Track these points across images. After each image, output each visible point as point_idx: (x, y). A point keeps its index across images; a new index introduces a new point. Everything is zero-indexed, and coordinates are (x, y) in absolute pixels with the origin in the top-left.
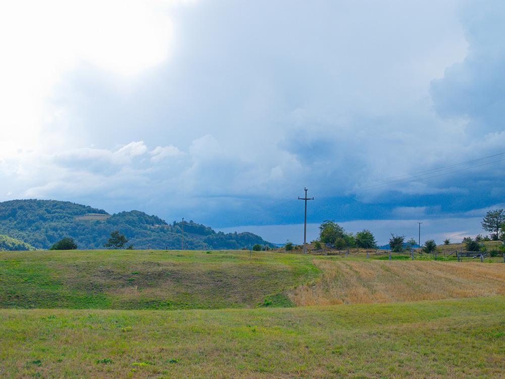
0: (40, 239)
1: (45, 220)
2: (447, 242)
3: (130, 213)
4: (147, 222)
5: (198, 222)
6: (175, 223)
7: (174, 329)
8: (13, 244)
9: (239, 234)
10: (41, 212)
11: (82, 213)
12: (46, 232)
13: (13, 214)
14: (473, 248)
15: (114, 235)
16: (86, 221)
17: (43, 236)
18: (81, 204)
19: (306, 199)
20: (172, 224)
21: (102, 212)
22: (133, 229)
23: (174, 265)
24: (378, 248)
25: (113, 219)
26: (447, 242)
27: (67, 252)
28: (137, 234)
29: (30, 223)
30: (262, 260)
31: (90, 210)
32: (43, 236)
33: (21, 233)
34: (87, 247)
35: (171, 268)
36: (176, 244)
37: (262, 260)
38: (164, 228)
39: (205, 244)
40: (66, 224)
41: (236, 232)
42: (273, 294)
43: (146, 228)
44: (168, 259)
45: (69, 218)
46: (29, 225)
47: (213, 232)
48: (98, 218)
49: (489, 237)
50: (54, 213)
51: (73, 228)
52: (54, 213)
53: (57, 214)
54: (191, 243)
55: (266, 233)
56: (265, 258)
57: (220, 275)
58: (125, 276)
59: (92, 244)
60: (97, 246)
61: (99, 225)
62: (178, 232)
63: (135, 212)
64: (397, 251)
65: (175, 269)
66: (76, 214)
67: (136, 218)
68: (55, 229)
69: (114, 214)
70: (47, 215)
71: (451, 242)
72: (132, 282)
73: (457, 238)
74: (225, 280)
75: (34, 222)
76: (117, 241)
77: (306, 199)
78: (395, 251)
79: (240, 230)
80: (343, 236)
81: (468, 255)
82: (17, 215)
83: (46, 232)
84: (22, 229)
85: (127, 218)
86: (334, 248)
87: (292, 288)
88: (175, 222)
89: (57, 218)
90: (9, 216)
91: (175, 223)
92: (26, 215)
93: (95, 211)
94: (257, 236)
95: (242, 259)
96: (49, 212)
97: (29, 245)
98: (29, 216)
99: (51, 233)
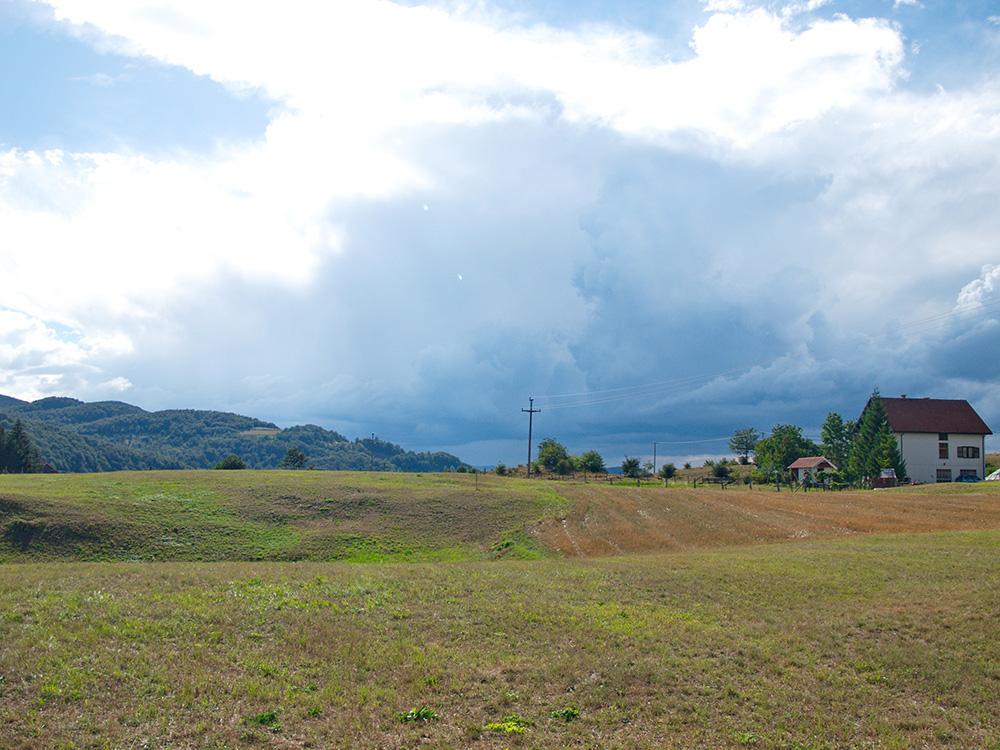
0: (197, 456)
1: (203, 434)
2: (688, 466)
3: (304, 428)
4: (325, 439)
5: (384, 439)
6: (357, 441)
7: (491, 615)
8: (166, 462)
9: (826, 440)
10: (199, 425)
11: (249, 428)
12: (205, 448)
13: (167, 425)
14: (721, 474)
15: (291, 453)
16: (252, 436)
17: (201, 453)
18: (246, 415)
19: (531, 412)
20: (354, 441)
21: (271, 426)
22: (307, 445)
23: (379, 491)
24: (605, 471)
25: (284, 434)
26: (688, 466)
27: (846, 500)
28: (313, 452)
29: (186, 437)
30: (489, 486)
31: (257, 424)
32: (201, 453)
33: (175, 449)
34: (253, 467)
35: (374, 495)
36: (357, 465)
37: (489, 486)
38: (344, 445)
39: (393, 465)
40: (228, 440)
41: (429, 453)
42: (512, 531)
43: (323, 446)
44: (366, 481)
45: (232, 432)
46: (185, 440)
47: (402, 451)
48: (266, 433)
49: (737, 460)
50: (214, 426)
51: (236, 445)
52: (214, 426)
53: (218, 427)
54: (377, 464)
55: (467, 454)
56: (493, 484)
57: (439, 504)
58: (315, 505)
59: (259, 464)
60: (265, 466)
61: (267, 442)
62: (361, 450)
63: (310, 426)
64: (632, 476)
65: (380, 495)
66: (241, 428)
67: (311, 434)
68: (215, 445)
69: (286, 429)
70: (206, 428)
71: (692, 466)
72: (325, 513)
73: (698, 461)
74: (446, 510)
75: (191, 436)
76: (296, 460)
77: (531, 412)
78: (629, 476)
79: (434, 450)
80: (566, 458)
81: (716, 482)
82: (171, 427)
83: (205, 448)
84: (176, 445)
85: (301, 433)
86: (555, 471)
87: (535, 522)
88: (357, 439)
89: (218, 432)
90: (162, 427)
91: (357, 441)
92: (181, 428)
93: (263, 425)
94: (453, 457)
95: (464, 484)
96: (208, 425)
97: (184, 464)
98: (185, 428)
99: (210, 449)
